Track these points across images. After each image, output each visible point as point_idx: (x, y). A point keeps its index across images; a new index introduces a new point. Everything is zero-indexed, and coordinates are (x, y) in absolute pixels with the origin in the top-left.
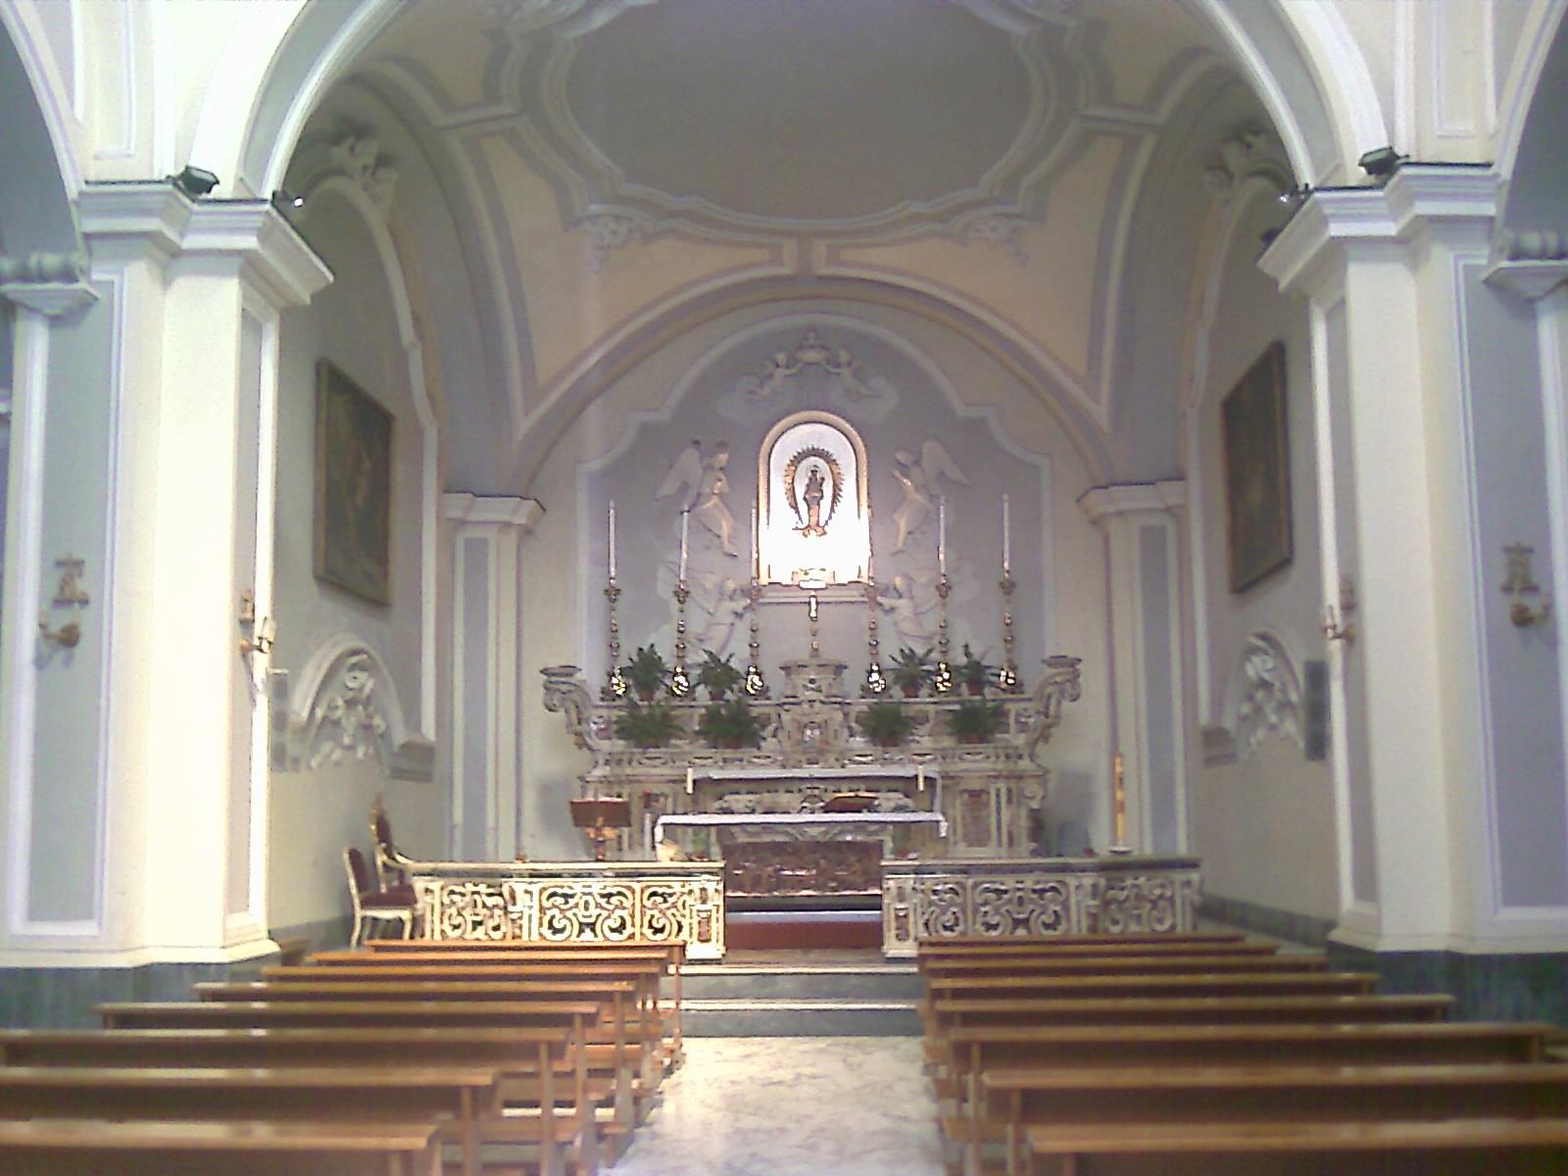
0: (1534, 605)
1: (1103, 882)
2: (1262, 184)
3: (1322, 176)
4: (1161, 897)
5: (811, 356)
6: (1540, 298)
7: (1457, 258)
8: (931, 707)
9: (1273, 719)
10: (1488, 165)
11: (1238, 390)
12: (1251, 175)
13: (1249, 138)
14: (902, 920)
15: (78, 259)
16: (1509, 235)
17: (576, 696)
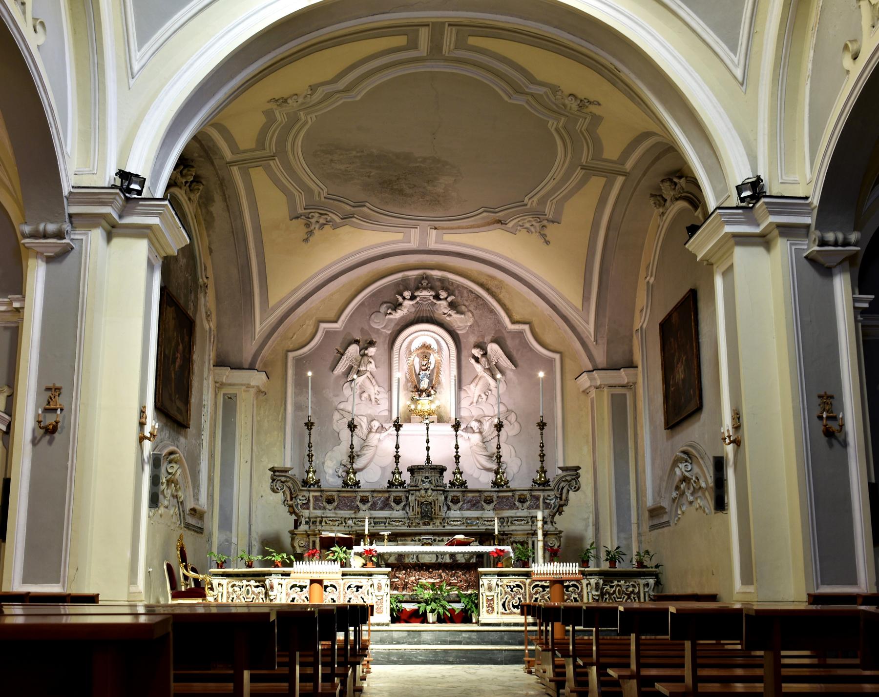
0: (834, 426)
1: (601, 582)
2: (682, 204)
3: (721, 201)
4: (633, 592)
5: (425, 293)
6: (835, 266)
7: (791, 244)
8: (495, 495)
9: (691, 498)
10: (806, 198)
11: (669, 316)
12: (677, 199)
13: (675, 180)
14: (490, 601)
15: (67, 227)
16: (818, 233)
17: (289, 484)
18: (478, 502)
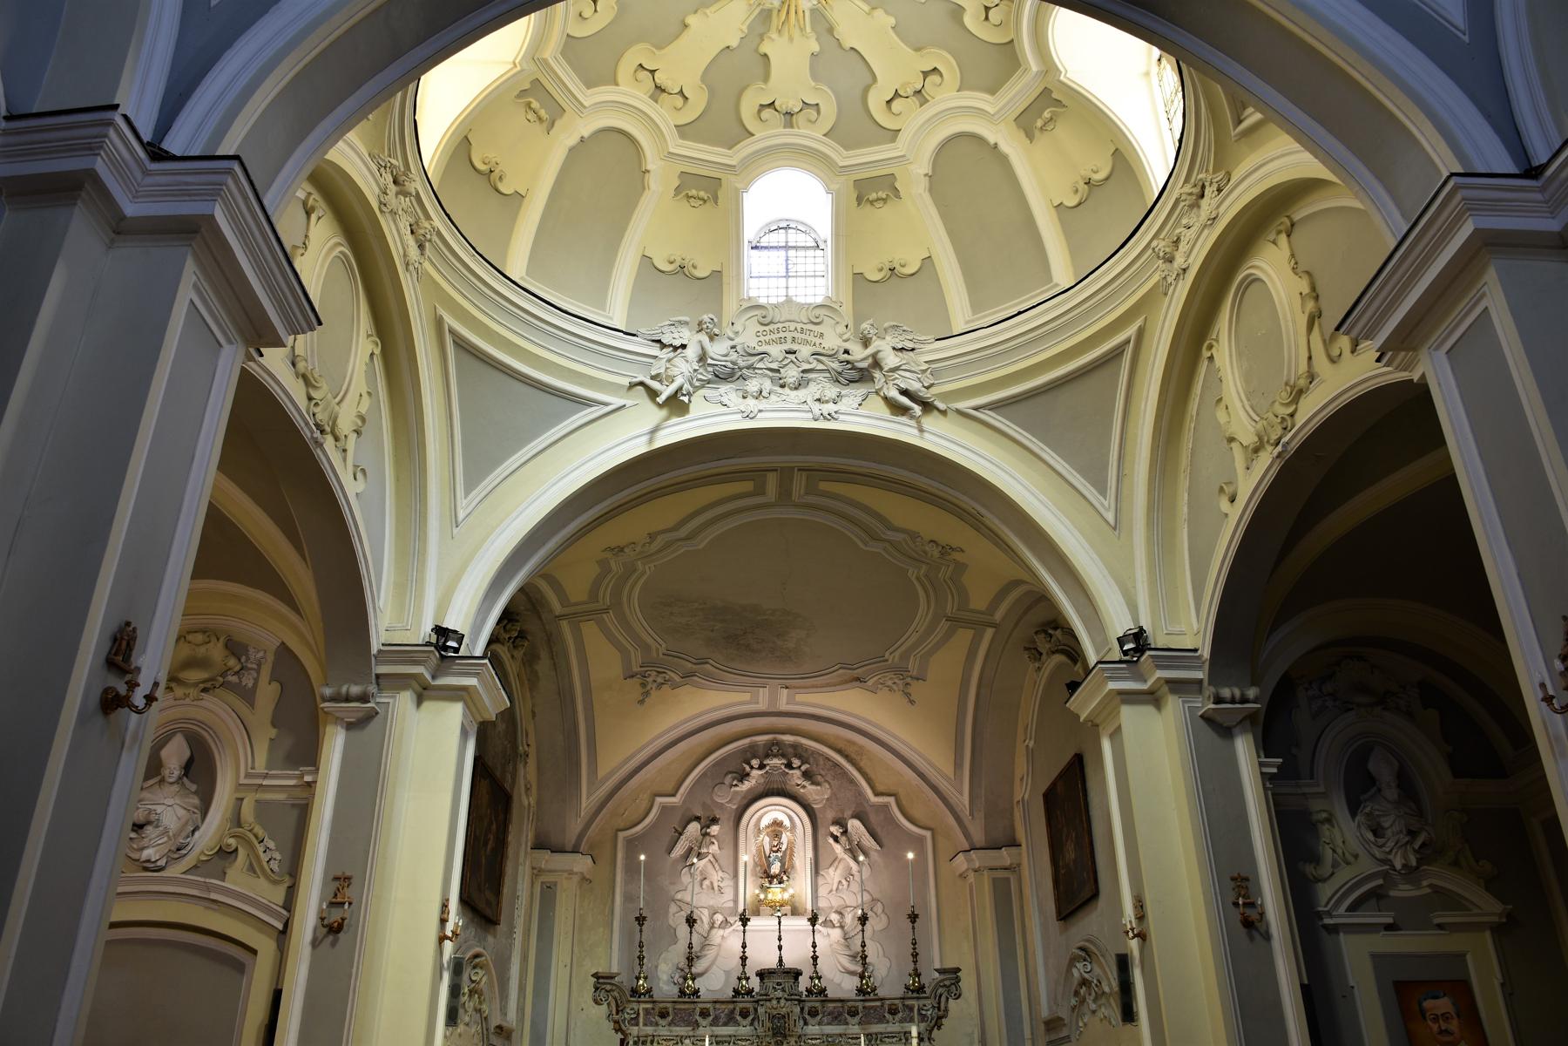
5: (776, 762)
8: (860, 1005)
9: (1093, 1006)
10: (1195, 650)
11: (1054, 784)
15: (372, 688)
16: (1212, 689)
18: (840, 1014)
